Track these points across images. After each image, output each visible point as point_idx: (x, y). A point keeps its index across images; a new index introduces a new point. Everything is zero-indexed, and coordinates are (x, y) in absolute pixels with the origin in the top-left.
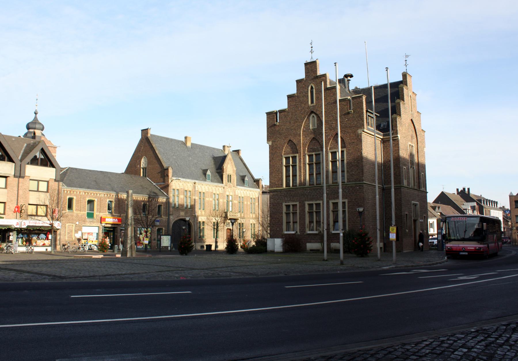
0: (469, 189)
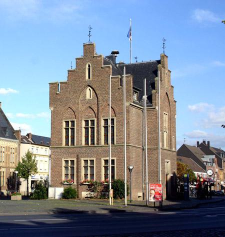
0: (208, 142)
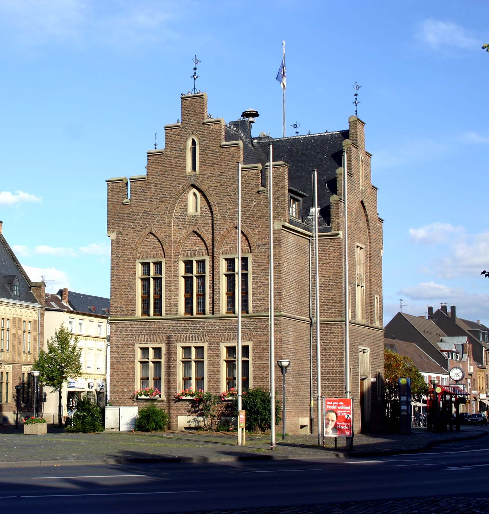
0: (453, 308)
